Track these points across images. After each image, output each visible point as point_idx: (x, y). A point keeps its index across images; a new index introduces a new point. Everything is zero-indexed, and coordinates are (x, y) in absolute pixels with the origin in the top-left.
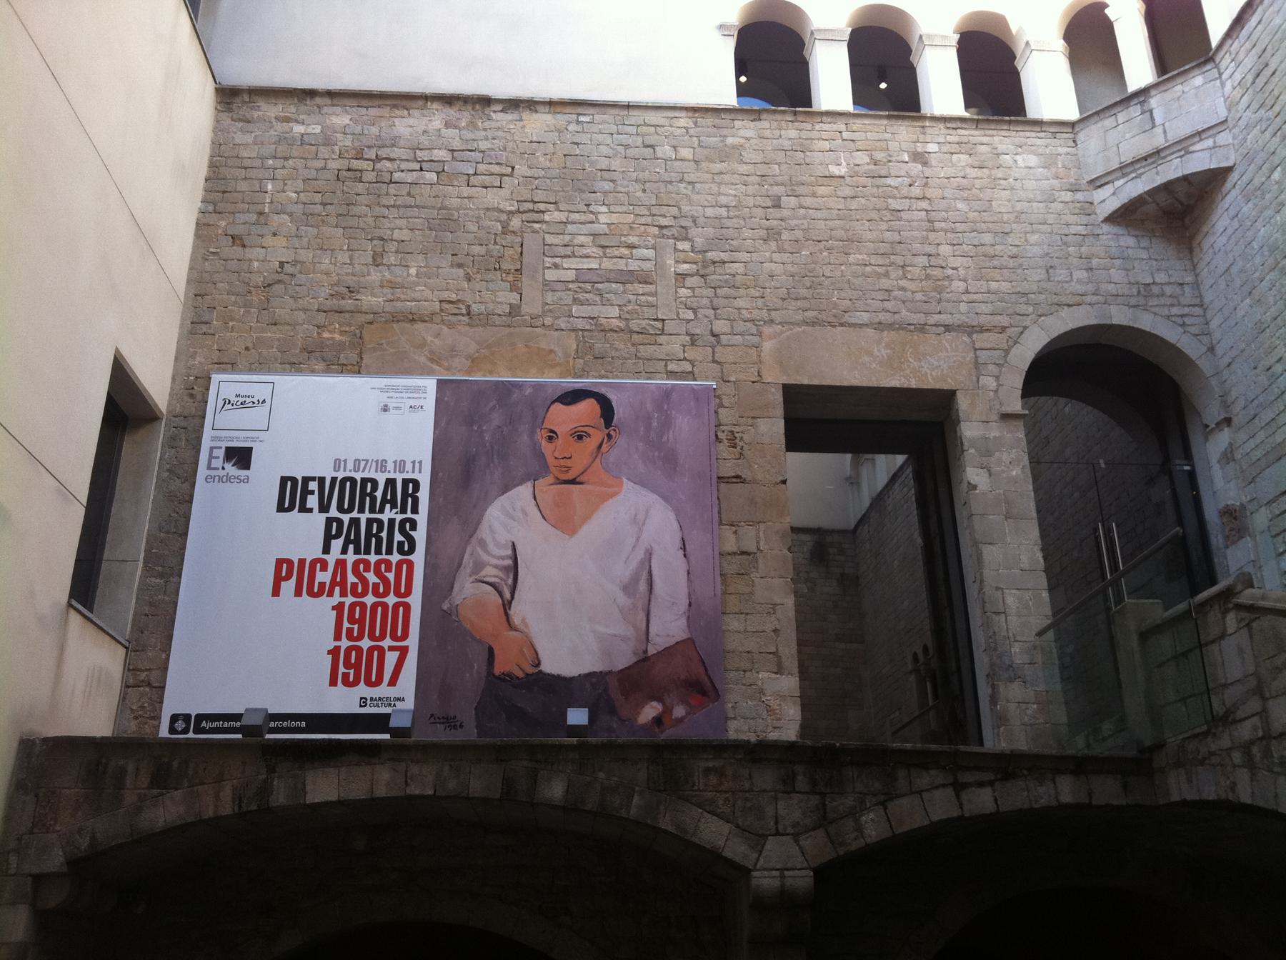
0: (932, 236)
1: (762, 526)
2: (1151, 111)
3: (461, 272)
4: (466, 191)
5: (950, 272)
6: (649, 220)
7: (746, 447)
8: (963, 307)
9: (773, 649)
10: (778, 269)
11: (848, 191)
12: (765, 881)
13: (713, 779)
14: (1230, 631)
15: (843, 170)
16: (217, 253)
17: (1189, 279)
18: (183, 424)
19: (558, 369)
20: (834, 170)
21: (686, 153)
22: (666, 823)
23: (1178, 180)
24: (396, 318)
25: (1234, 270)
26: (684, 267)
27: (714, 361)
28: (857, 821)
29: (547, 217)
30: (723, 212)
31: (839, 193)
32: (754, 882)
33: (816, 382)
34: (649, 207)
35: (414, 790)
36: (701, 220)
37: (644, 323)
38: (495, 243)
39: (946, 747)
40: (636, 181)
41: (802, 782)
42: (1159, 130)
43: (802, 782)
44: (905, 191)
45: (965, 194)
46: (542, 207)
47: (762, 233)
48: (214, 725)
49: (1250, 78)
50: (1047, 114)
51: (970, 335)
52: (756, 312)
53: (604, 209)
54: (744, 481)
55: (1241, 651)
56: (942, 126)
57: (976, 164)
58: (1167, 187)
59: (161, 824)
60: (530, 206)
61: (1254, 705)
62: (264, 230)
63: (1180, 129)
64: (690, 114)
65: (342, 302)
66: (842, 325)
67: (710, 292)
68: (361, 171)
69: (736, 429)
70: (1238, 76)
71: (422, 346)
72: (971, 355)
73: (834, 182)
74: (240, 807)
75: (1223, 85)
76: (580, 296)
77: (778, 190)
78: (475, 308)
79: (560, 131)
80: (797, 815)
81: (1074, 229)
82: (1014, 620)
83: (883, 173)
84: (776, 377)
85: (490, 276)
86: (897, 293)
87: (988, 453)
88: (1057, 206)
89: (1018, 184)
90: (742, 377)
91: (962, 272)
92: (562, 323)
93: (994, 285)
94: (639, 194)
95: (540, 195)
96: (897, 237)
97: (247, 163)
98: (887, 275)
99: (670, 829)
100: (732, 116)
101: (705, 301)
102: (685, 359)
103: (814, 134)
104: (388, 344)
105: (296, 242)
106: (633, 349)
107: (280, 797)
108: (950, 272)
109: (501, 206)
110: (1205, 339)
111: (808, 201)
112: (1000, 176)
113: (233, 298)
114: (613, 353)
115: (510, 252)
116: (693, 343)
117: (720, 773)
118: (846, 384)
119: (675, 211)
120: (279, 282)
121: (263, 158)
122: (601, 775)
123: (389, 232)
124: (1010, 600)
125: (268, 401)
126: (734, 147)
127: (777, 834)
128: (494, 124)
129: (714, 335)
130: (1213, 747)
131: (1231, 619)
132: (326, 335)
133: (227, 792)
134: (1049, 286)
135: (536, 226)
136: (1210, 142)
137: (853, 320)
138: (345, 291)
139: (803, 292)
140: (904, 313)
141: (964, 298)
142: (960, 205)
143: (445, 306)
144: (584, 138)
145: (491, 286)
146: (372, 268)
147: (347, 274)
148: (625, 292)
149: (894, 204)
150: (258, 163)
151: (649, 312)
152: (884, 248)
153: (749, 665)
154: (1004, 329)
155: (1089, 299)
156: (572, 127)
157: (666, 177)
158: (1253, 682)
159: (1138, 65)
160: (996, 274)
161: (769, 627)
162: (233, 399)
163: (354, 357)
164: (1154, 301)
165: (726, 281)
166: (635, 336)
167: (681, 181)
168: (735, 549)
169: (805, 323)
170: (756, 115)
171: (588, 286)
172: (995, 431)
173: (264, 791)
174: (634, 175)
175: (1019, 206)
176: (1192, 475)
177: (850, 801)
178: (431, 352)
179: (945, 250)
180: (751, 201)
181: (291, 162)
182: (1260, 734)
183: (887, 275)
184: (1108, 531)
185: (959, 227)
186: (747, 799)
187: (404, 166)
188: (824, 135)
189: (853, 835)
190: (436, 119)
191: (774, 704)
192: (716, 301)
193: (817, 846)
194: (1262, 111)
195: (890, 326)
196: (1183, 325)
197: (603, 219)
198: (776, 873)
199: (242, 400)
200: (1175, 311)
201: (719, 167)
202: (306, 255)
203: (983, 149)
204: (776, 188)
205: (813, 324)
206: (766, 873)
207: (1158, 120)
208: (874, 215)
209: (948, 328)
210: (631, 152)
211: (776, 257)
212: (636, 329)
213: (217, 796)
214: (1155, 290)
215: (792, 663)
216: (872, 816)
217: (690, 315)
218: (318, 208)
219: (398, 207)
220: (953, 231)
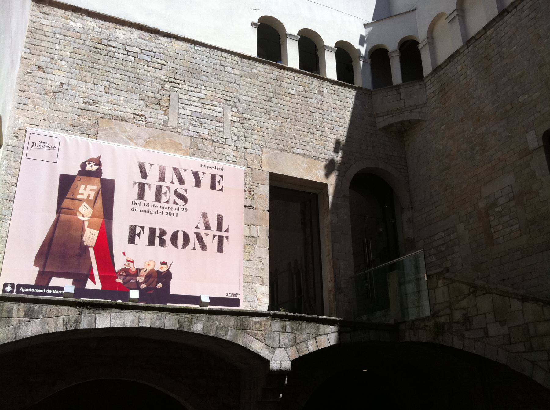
0: (323, 124)
1: (259, 227)
2: (400, 94)
3: (143, 103)
4: (147, 68)
5: (329, 139)
6: (222, 96)
7: (255, 195)
9: (260, 275)
11: (295, 101)
12: (274, 366)
13: (258, 326)
14: (440, 286)
15: (293, 92)
16: (31, 73)
18: (13, 149)
19: (183, 152)
20: (291, 91)
21: (237, 72)
22: (240, 342)
24: (114, 118)
26: (235, 119)
27: (245, 159)
28: (306, 344)
29: (180, 86)
30: (250, 99)
31: (293, 101)
32: (271, 365)
34: (222, 91)
35: (142, 325)
36: (241, 100)
37: (218, 138)
38: (158, 93)
39: (292, 314)
40: (217, 79)
41: (288, 329)
42: (402, 101)
43: (288, 329)
44: (315, 105)
45: (335, 110)
46: (179, 82)
48: (27, 290)
49: (437, 91)
50: (290, 65)
53: (204, 88)
54: (253, 208)
57: (339, 100)
58: (402, 123)
59: (29, 334)
60: (173, 80)
62: (55, 67)
65: (90, 106)
66: (291, 152)
67: (244, 130)
68: (100, 49)
69: (251, 187)
70: (433, 90)
71: (125, 132)
74: (66, 328)
75: (426, 91)
76: (193, 122)
77: (271, 95)
78: (148, 119)
79: (187, 51)
80: (287, 340)
83: (308, 96)
84: (267, 169)
85: (156, 106)
86: (310, 144)
90: (254, 167)
92: (185, 132)
94: (218, 85)
95: (177, 76)
97: (47, 34)
98: (307, 136)
99: (242, 344)
101: (242, 134)
102: (233, 156)
104: (110, 128)
105: (69, 75)
106: (213, 148)
107: (84, 324)
108: (329, 139)
109: (162, 78)
111: (281, 102)
112: (347, 106)
113: (38, 95)
114: (205, 149)
115: (164, 98)
116: (237, 150)
117: (260, 323)
118: (291, 175)
119: (231, 95)
120: (60, 92)
121: (55, 33)
122: (217, 322)
123: (112, 79)
125: (57, 147)
126: (255, 74)
127: (280, 348)
128: (160, 42)
129: (245, 148)
130: (427, 324)
131: (440, 282)
132: (82, 120)
133: (61, 321)
135: (176, 89)
136: (419, 110)
137: (295, 151)
138: (91, 101)
139: (278, 137)
143: (136, 116)
144: (197, 56)
145: (156, 111)
146: (104, 94)
147: (92, 94)
148: (211, 124)
149: (312, 109)
150: (52, 35)
151: (220, 134)
153: (251, 281)
156: (192, 50)
157: (228, 79)
159: (397, 77)
161: (260, 267)
162: (38, 143)
163: (94, 132)
165: (250, 127)
166: (214, 143)
167: (235, 83)
168: (249, 235)
169: (278, 149)
170: (263, 63)
171: (196, 119)
173: (78, 321)
174: (216, 76)
177: (304, 336)
178: (129, 135)
180: (260, 97)
181: (68, 38)
182: (448, 321)
183: (307, 136)
185: (333, 123)
186: (269, 334)
187: (120, 51)
188: (288, 77)
189: (305, 349)
190: (136, 34)
191: (260, 297)
192: (246, 135)
193: (293, 353)
195: (308, 156)
197: (203, 91)
198: (279, 362)
199: (43, 145)
201: (249, 80)
202: (73, 82)
203: (341, 94)
204: (270, 94)
205: (281, 150)
206: (275, 362)
207: (402, 97)
210: (215, 66)
212: (215, 140)
213: (56, 323)
215: (267, 281)
216: (311, 342)
217: (236, 138)
218: (80, 62)
219: (117, 69)
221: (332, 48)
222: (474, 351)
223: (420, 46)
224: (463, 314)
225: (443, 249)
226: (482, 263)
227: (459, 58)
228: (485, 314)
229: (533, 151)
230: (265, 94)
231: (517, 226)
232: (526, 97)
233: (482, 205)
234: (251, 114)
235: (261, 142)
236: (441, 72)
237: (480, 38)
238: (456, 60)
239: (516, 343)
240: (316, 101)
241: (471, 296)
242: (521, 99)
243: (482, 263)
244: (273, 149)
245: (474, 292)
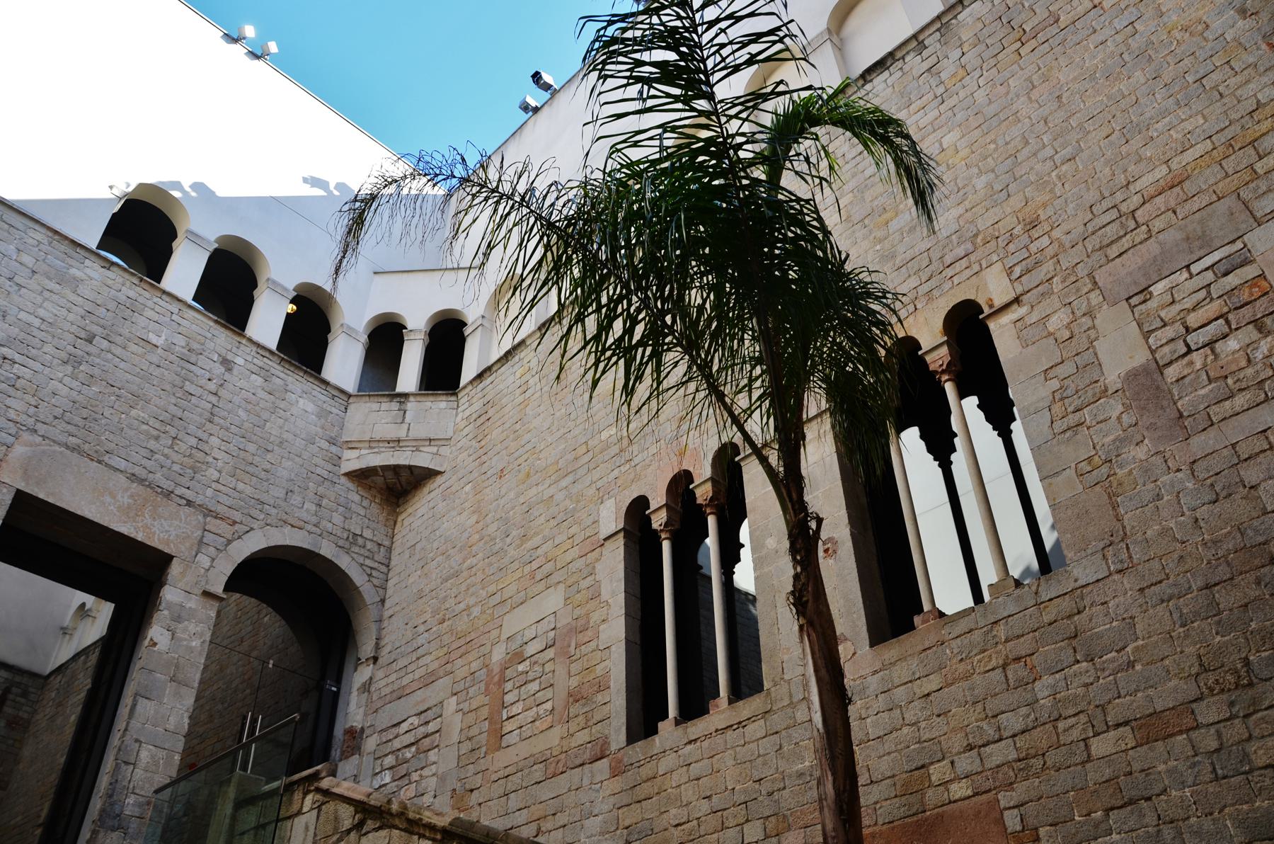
5: (210, 459)
8: (209, 492)
10: (64, 391)
11: (155, 359)
15: (160, 342)
17: (387, 543)
20: (153, 338)
21: (26, 259)
23: (405, 466)
25: (418, 547)
30: (37, 322)
33: (140, 537)
44: (203, 382)
47: (64, 355)
51: (205, 516)
52: (24, 417)
56: (254, 349)
58: (396, 469)
63: (419, 431)
64: (50, 234)
66: (100, 462)
70: (467, 413)
72: (199, 533)
73: (149, 347)
75: (457, 415)
77: (95, 329)
81: (319, 471)
82: (139, 773)
87: (178, 619)
88: (314, 449)
89: (293, 419)
91: (220, 464)
93: (240, 486)
96: (179, 413)
98: (157, 438)
100: (87, 255)
103: (150, 303)
110: (381, 591)
111: (118, 351)
118: (79, 513)
124: (144, 755)
134: (283, 504)
136: (434, 449)
139: (77, 420)
140: (158, 475)
141: (214, 485)
142: (241, 412)
149: (189, 387)
152: (164, 416)
154: (235, 522)
155: (309, 527)
160: (246, 478)
164: (356, 549)
165: (8, 379)
167: (10, 279)
172: (193, 603)
175: (285, 436)
176: (336, 696)
179: (214, 441)
184: (254, 721)
188: (157, 308)
194: (474, 442)
196: (370, 575)
200: (368, 562)
201: (52, 285)
205: (73, 450)
207: (408, 419)
208: (168, 387)
209: (189, 503)
211: (67, 380)
214: (360, 541)
220: (227, 429)
221: (286, 289)
223: (467, 331)
225: (408, 755)
226: (472, 791)
227: (523, 354)
230: (82, 323)
231: (548, 706)
233: (498, 655)
234: (25, 352)
235: (22, 418)
236: (489, 380)
238: (517, 358)
240: (208, 375)
242: (604, 435)
243: (472, 791)
244: (54, 441)
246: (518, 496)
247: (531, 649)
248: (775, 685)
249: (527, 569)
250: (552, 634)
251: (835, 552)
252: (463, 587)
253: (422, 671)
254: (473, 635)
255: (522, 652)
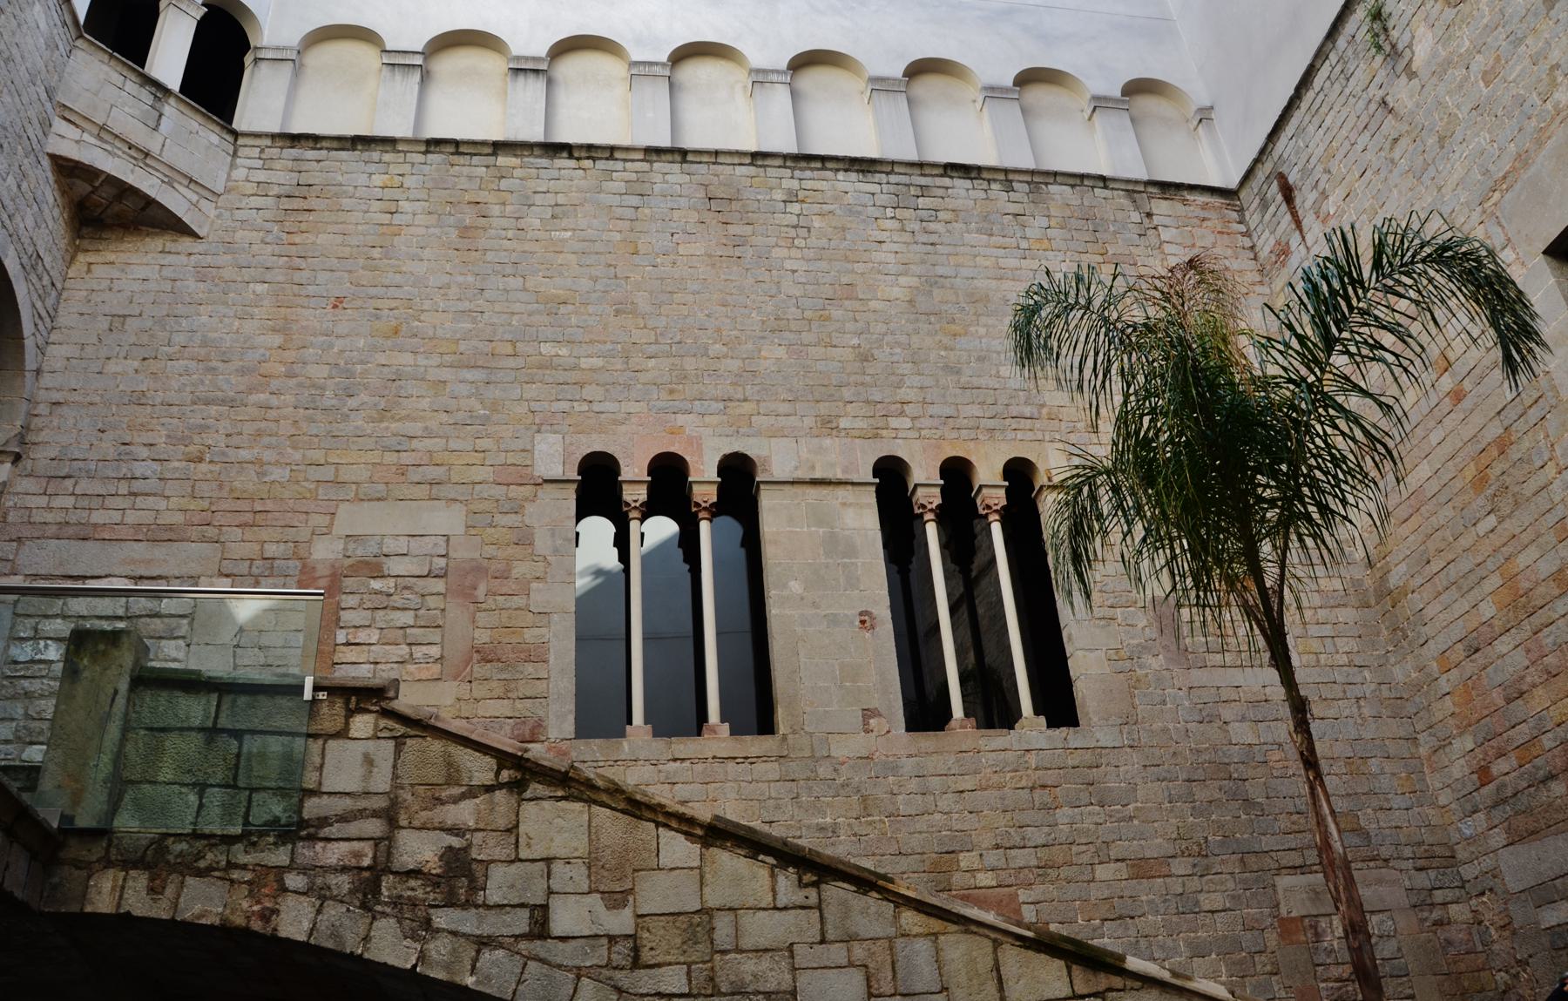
55: (369, 761)
61: (374, 827)
75: (233, 166)
130: (243, 859)
131: (362, 724)
136: (195, 198)
158: (380, 803)
182: (366, 862)
222: (470, 981)
224: (450, 848)
228: (548, 861)
229: (546, 481)
231: (435, 651)
232: (564, 351)
237: (472, 155)
239: (659, 965)
241: (500, 795)
245: (517, 787)
246: (374, 349)
247: (396, 566)
248: (794, 732)
249: (390, 458)
250: (442, 562)
251: (873, 627)
252: (248, 428)
253: (147, 517)
254: (269, 506)
255: (379, 567)
